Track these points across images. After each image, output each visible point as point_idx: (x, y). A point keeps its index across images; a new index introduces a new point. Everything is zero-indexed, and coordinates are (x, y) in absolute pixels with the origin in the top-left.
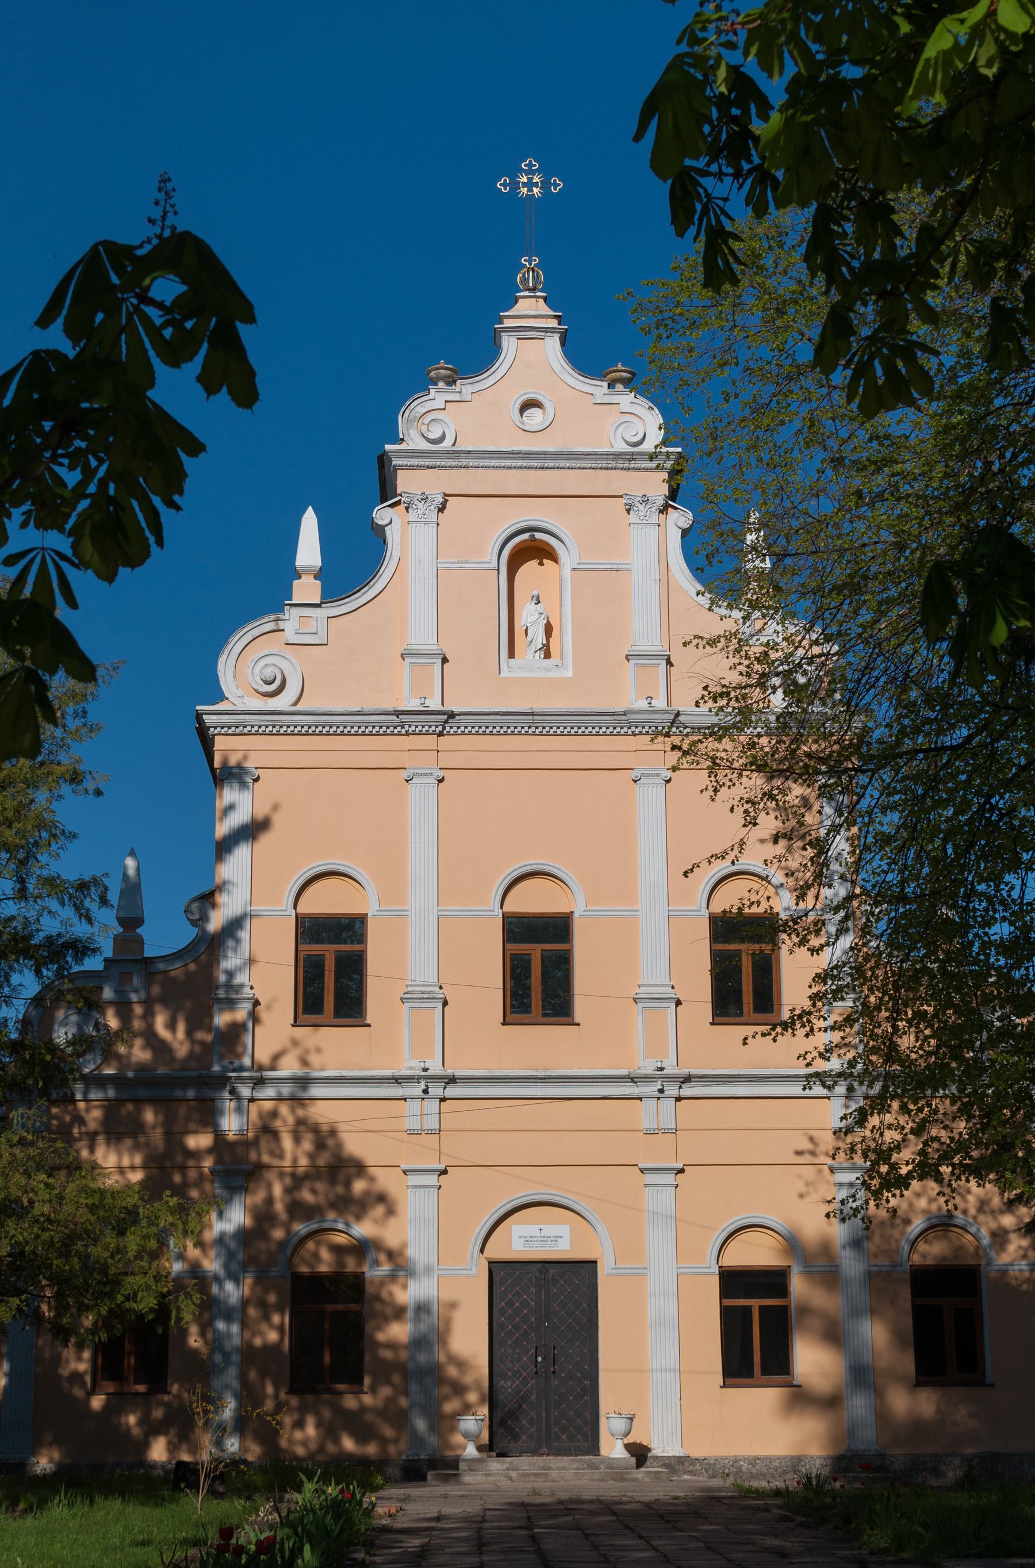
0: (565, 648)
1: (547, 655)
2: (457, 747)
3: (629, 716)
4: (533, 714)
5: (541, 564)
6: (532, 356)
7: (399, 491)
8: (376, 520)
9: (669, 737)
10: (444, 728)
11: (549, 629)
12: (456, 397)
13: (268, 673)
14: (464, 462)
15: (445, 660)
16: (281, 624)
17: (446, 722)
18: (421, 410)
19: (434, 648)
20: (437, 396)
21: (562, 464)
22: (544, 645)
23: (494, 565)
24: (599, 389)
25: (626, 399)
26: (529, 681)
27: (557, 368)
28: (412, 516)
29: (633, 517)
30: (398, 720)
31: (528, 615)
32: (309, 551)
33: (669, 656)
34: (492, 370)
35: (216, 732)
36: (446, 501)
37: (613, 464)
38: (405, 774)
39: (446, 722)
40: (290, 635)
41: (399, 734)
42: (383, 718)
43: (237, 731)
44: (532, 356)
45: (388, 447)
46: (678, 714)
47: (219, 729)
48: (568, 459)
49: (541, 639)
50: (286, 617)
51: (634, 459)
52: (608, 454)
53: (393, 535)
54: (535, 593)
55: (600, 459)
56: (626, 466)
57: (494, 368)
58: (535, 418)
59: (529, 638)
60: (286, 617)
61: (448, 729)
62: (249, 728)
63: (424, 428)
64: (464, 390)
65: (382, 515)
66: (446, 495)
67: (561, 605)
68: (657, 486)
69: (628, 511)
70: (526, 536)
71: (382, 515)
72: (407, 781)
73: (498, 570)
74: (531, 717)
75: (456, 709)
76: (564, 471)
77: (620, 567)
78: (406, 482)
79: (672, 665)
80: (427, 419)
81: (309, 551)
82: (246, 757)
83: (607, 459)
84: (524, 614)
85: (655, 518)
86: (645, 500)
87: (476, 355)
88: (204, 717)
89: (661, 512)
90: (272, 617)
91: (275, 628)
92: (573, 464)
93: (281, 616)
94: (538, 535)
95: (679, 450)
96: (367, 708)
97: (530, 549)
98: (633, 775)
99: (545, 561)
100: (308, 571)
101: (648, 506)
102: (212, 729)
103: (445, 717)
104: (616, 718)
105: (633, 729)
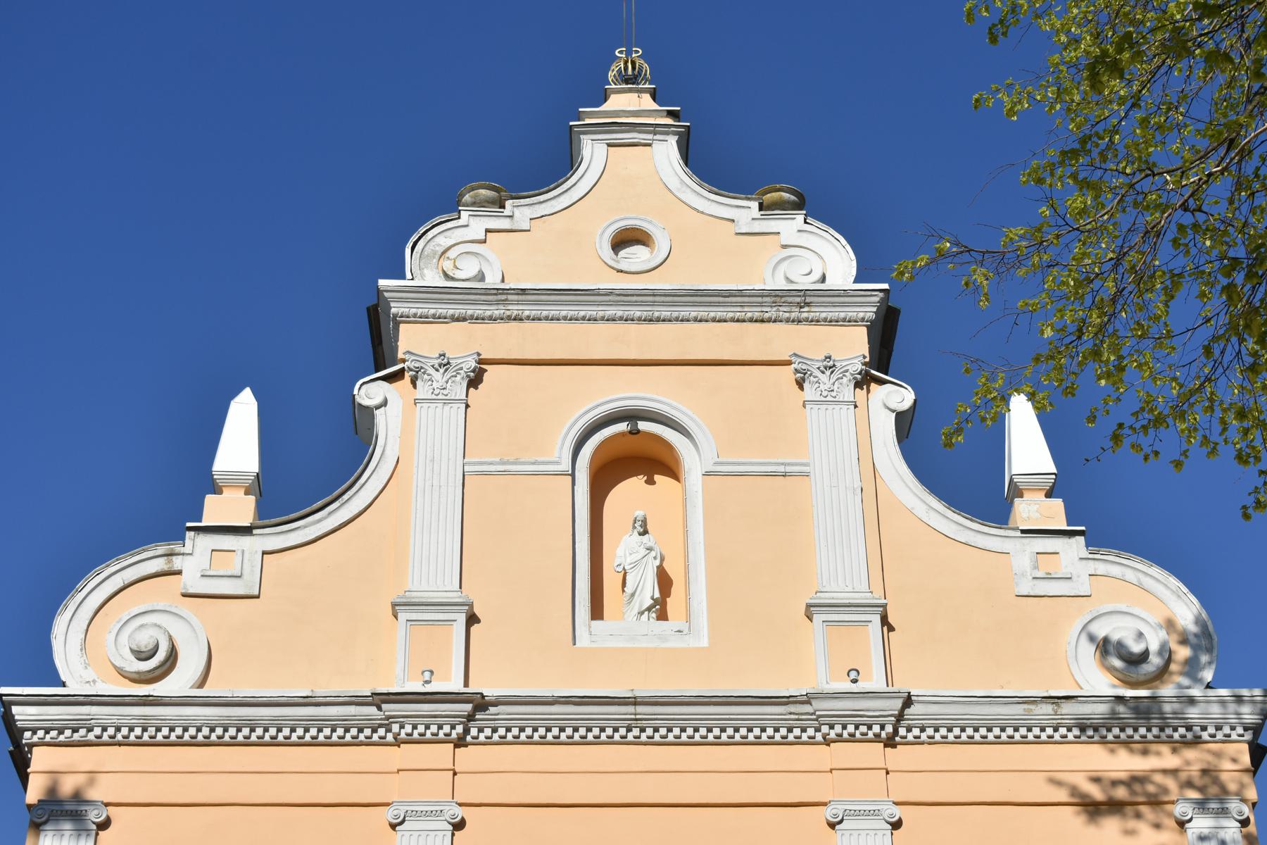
0: (694, 603)
1: (663, 616)
2: (491, 766)
3: (817, 704)
4: (635, 702)
5: (650, 482)
6: (632, 170)
7: (400, 355)
8: (358, 399)
9: (894, 746)
10: (467, 731)
11: (664, 581)
12: (505, 224)
13: (144, 640)
14: (514, 310)
15: (472, 619)
16: (177, 563)
17: (470, 718)
18: (444, 241)
19: (455, 597)
20: (472, 224)
21: (685, 312)
22: (656, 601)
23: (566, 465)
24: (746, 212)
25: (792, 226)
26: (624, 652)
27: (674, 183)
28: (423, 390)
29: (810, 392)
30: (380, 715)
31: (623, 549)
32: (239, 444)
33: (884, 606)
34: (565, 186)
35: (35, 739)
36: (483, 371)
37: (772, 313)
38: (390, 814)
39: (470, 718)
40: (191, 580)
41: (382, 743)
42: (352, 710)
43: (73, 737)
44: (632, 170)
45: (382, 283)
46: (908, 701)
47: (41, 733)
48: (694, 304)
49: (649, 591)
50: (188, 549)
51: (808, 304)
52: (763, 294)
53: (387, 425)
54: (639, 514)
55: (751, 305)
56: (793, 315)
57: (569, 183)
58: (636, 256)
59: (629, 589)
60: (188, 549)
61: (474, 732)
62: (98, 731)
63: (447, 266)
64: (517, 212)
65: (369, 392)
66: (481, 362)
67: (686, 532)
68: (854, 346)
69: (800, 384)
70: (622, 427)
71: (369, 392)
72: (393, 826)
73: (573, 475)
74: (631, 709)
75: (490, 692)
76: (686, 325)
77: (789, 469)
78: (411, 341)
79: (891, 629)
80: (452, 254)
81: (239, 444)
82: (91, 782)
83: (761, 305)
84: (620, 551)
85: (847, 392)
86: (829, 366)
87: (541, 165)
88: (15, 709)
89: (858, 385)
90: (161, 549)
91: (166, 568)
92: (701, 312)
93: (177, 548)
94: (643, 426)
95: (886, 286)
96: (321, 691)
97: (630, 454)
98: (829, 813)
99: (657, 477)
100: (234, 480)
101: (834, 376)
102: (27, 734)
103: (469, 707)
104: (792, 708)
105: (825, 729)
